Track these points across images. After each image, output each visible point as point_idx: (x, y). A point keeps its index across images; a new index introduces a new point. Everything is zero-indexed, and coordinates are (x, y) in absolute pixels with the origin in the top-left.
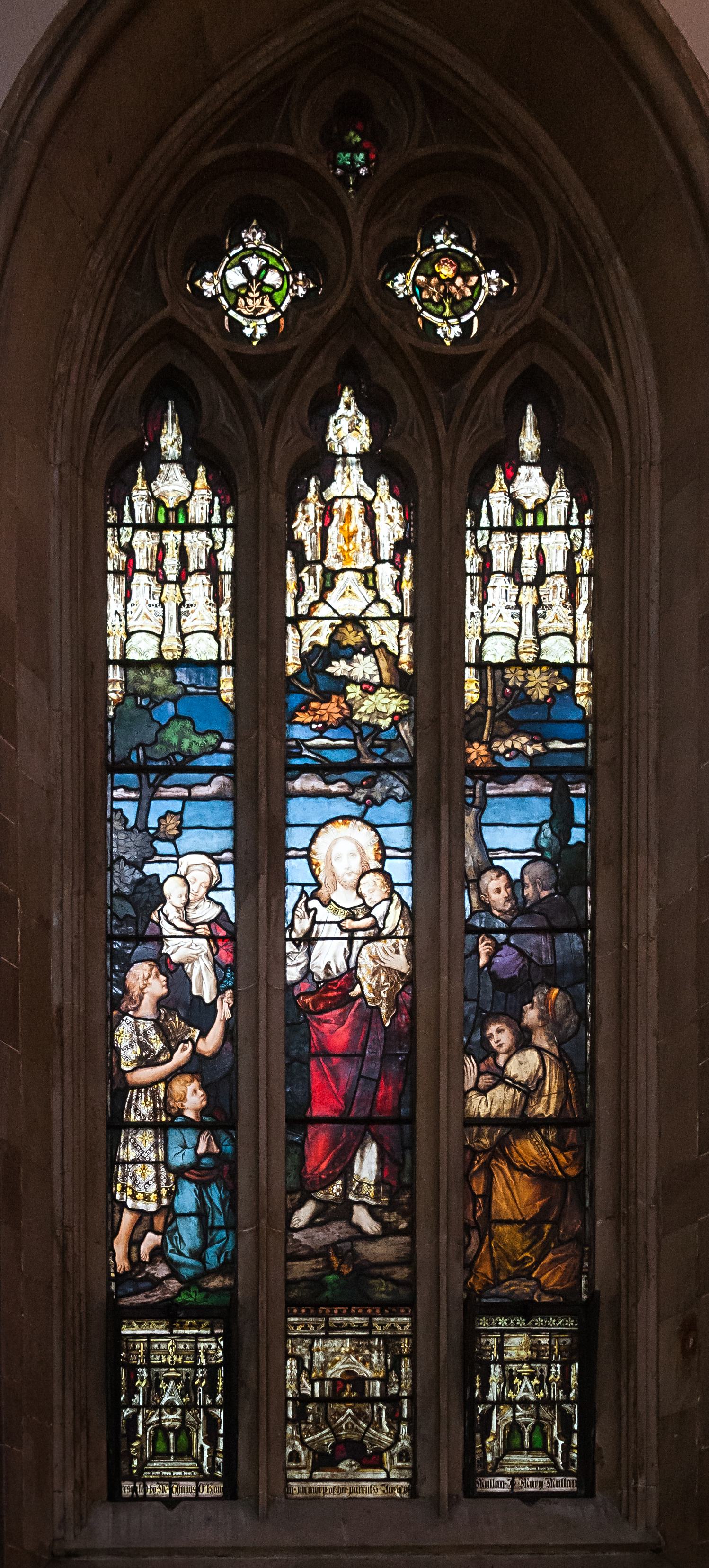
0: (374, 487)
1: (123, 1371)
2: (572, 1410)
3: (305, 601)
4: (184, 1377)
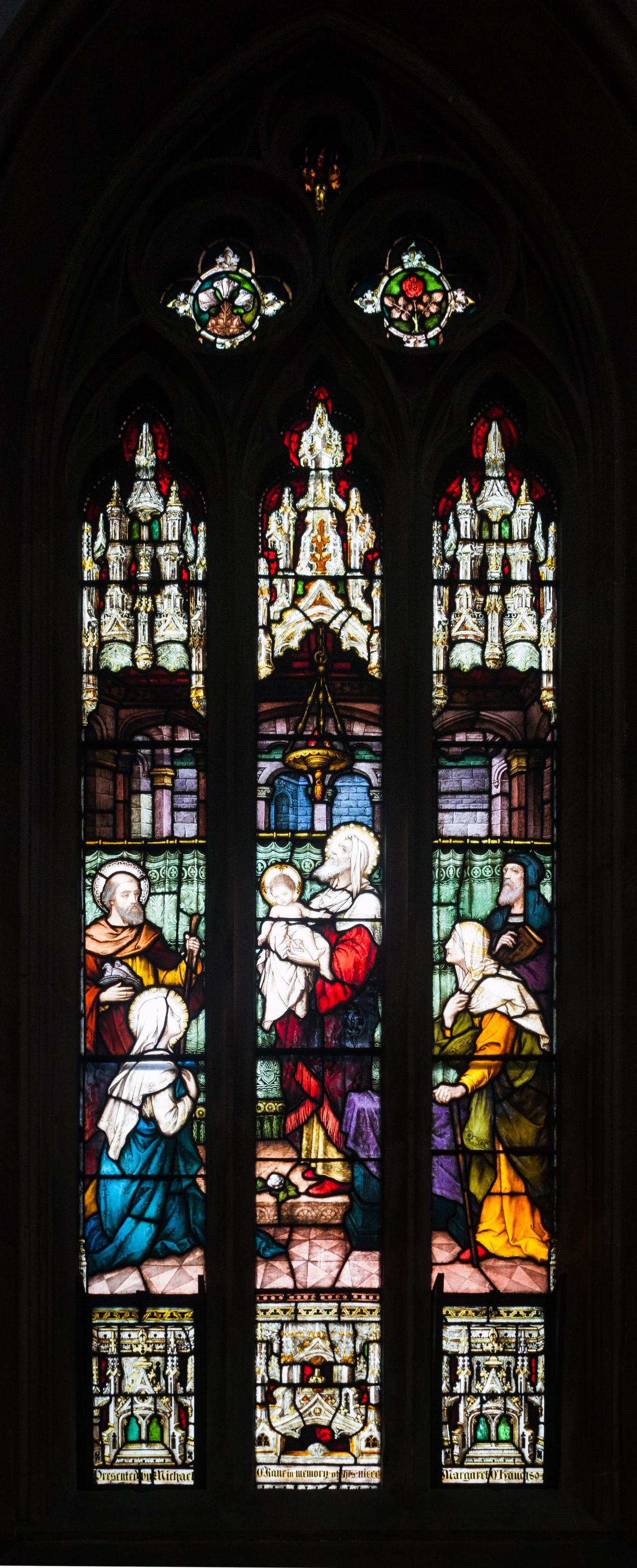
0: (347, 500)
1: (95, 1361)
2: (539, 1404)
3: (276, 608)
4: (505, 1366)
